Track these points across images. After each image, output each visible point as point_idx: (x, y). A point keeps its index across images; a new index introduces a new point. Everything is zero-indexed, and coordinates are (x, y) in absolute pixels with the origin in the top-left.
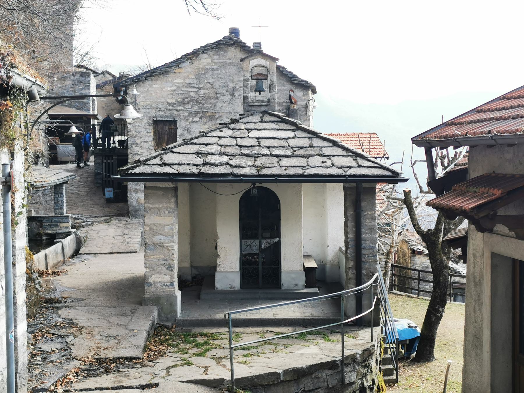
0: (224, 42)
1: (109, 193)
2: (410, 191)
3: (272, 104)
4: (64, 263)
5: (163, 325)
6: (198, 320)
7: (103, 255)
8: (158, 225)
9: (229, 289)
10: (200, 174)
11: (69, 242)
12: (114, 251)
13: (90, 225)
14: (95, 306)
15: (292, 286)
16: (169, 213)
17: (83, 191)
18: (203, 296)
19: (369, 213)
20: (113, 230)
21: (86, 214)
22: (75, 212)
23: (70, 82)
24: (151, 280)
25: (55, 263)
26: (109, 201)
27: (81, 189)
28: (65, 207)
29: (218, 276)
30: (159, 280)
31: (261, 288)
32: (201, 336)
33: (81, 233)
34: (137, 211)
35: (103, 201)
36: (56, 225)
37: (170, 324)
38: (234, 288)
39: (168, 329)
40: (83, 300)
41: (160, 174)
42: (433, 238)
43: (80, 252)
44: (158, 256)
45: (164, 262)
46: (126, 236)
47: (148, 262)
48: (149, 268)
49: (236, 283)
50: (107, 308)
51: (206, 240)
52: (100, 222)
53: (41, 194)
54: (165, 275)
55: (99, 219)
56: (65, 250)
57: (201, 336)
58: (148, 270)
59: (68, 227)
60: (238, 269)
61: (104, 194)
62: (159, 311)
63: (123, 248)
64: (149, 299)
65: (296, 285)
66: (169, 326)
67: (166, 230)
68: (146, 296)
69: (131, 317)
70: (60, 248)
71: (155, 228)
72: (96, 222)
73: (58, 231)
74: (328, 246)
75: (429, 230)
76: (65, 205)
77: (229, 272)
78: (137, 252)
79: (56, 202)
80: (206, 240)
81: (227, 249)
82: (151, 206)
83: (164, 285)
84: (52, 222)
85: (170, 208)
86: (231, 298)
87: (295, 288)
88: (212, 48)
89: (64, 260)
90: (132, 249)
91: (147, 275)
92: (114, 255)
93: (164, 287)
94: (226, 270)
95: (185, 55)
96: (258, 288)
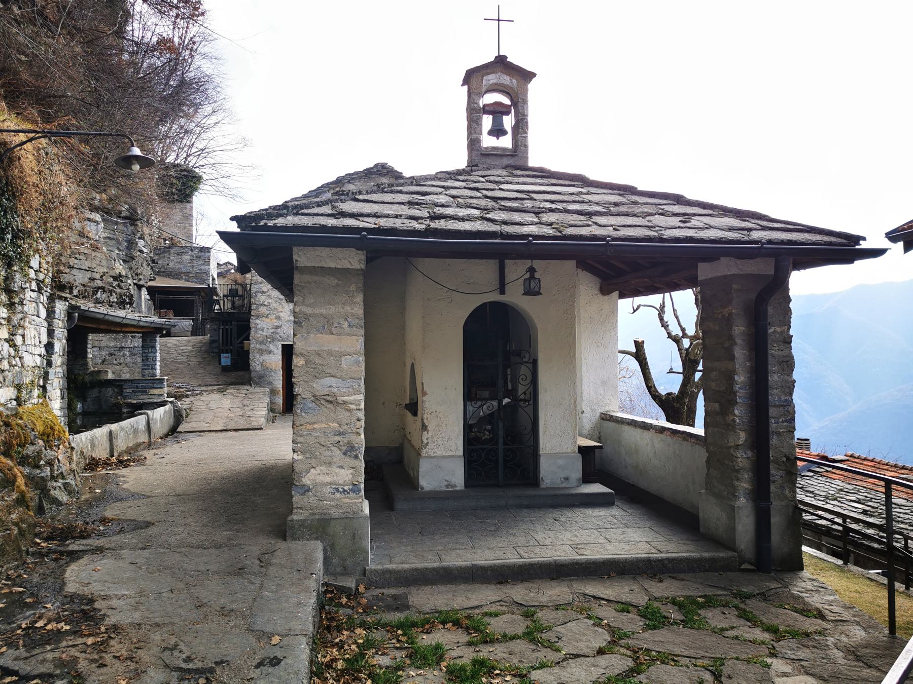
0: (375, 170)
1: (226, 359)
2: (643, 342)
3: (521, 155)
4: (149, 445)
5: (337, 587)
6: (417, 570)
7: (213, 434)
8: (325, 354)
9: (444, 489)
10: (429, 232)
11: (160, 416)
12: (229, 428)
13: (197, 395)
14: (170, 547)
15: (559, 481)
16: (350, 326)
17: (194, 362)
18: (399, 505)
19: (778, 329)
20: (229, 401)
21: (194, 382)
22: (179, 380)
23: (188, 257)
24: (306, 481)
25: (131, 445)
26: (225, 369)
27: (192, 359)
28: (158, 367)
29: (424, 467)
30: (328, 479)
31: (501, 487)
32: (444, 623)
33: (182, 404)
34: (261, 377)
35: (218, 370)
36: (144, 392)
37: (350, 583)
38: (455, 486)
39: (348, 597)
40: (148, 524)
41: (334, 229)
42: (677, 405)
43: (178, 430)
44: (323, 425)
45: (337, 438)
46: (246, 408)
47: (300, 439)
48: (303, 453)
49: (456, 476)
50: (200, 551)
51: (384, 404)
52: (212, 391)
53: (127, 353)
54: (341, 467)
55: (210, 388)
56: (152, 426)
57: (444, 623)
58: (300, 457)
59: (162, 395)
60: (461, 453)
61: (220, 364)
62: (325, 550)
63: (242, 424)
64: (302, 523)
65: (567, 479)
66: (350, 589)
67: (344, 366)
68: (295, 517)
69: (258, 581)
70: (144, 423)
71: (317, 360)
72: (206, 391)
73: (146, 401)
74: (583, 412)
75: (669, 394)
76: (158, 363)
77: (444, 457)
78: (261, 429)
79: (145, 359)
80: (384, 404)
81: (440, 415)
82: (309, 311)
83: (337, 490)
84: (137, 387)
85: (353, 315)
86: (447, 510)
87: (564, 485)
88: (360, 178)
89: (150, 442)
90: (255, 424)
91: (298, 467)
92: (229, 433)
93: (338, 495)
94: (439, 453)
95: (327, 184)
96: (497, 486)
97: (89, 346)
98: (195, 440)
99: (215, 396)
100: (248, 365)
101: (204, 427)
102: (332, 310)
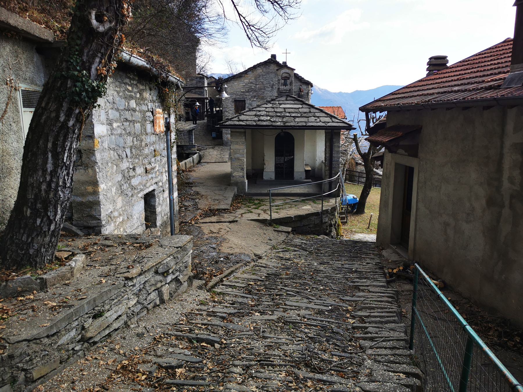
1: (214, 135)
4: (194, 166)
10: (257, 125)
24: (233, 175)
26: (214, 139)
33: (201, 153)
34: (227, 143)
36: (190, 149)
41: (238, 125)
49: (273, 177)
52: (210, 148)
63: (221, 160)
97: (312, 236)
98: (208, 166)
99: (211, 150)
100: (222, 138)
101: (209, 161)
102: (238, 140)
